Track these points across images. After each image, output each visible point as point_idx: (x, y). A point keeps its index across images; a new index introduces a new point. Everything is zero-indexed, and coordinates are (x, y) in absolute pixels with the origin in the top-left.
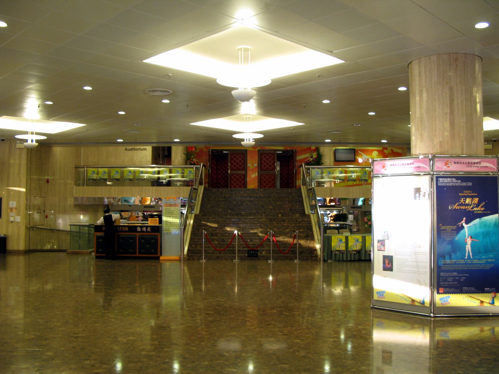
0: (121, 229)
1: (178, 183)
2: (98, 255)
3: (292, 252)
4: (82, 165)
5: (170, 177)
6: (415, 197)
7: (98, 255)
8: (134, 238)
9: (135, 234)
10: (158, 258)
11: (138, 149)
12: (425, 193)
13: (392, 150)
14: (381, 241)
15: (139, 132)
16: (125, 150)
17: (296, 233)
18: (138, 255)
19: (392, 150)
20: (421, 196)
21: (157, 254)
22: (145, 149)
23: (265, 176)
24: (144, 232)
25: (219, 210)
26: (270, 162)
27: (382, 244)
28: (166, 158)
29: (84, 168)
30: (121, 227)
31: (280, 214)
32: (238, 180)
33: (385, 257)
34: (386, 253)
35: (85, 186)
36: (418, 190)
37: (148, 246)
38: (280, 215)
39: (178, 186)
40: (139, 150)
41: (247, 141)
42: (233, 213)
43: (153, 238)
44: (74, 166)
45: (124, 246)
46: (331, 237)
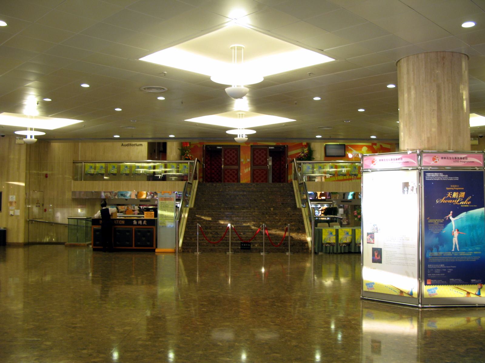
0: (117, 223)
1: (173, 178)
2: (95, 247)
3: (284, 245)
4: (79, 160)
5: (165, 172)
6: (404, 191)
7: (95, 247)
8: (130, 231)
9: (131, 227)
10: (154, 251)
11: (135, 144)
12: (413, 187)
13: (381, 146)
14: (371, 234)
16: (122, 145)
17: (288, 226)
18: (134, 247)
19: (381, 146)
20: (410, 190)
21: (152, 246)
22: (141, 144)
23: (258, 171)
24: (139, 225)
25: (213, 204)
26: (263, 157)
27: (371, 237)
28: (161, 153)
29: (82, 163)
30: (117, 221)
31: (272, 207)
32: (231, 174)
33: (374, 250)
34: (375, 246)
35: (83, 180)
36: (406, 185)
37: (144, 239)
38: (272, 209)
39: (173, 181)
40: (135, 145)
41: (240, 137)
42: (226, 206)
43: (149, 231)
44: (72, 161)
45: (121, 239)
46: (322, 230)
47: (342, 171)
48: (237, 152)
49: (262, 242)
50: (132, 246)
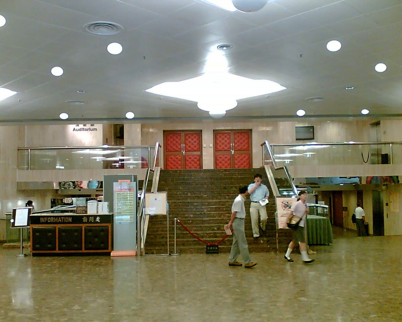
0: (63, 221)
1: (131, 166)
2: (34, 252)
3: (267, 242)
4: (26, 147)
5: (123, 160)
7: (34, 252)
8: (79, 231)
9: (81, 225)
10: (109, 254)
11: (88, 129)
15: (84, 104)
16: (74, 130)
18: (84, 251)
21: (108, 249)
22: (95, 129)
23: (221, 156)
24: (91, 223)
25: (178, 193)
26: (226, 141)
28: (118, 139)
29: (28, 149)
30: (62, 218)
32: (193, 161)
35: (29, 169)
37: (96, 240)
39: (117, 168)
40: (89, 130)
42: (193, 195)
43: (103, 231)
44: (17, 149)
45: (70, 239)
47: (116, 165)
48: (230, 137)
49: (173, 240)
50: (55, 250)
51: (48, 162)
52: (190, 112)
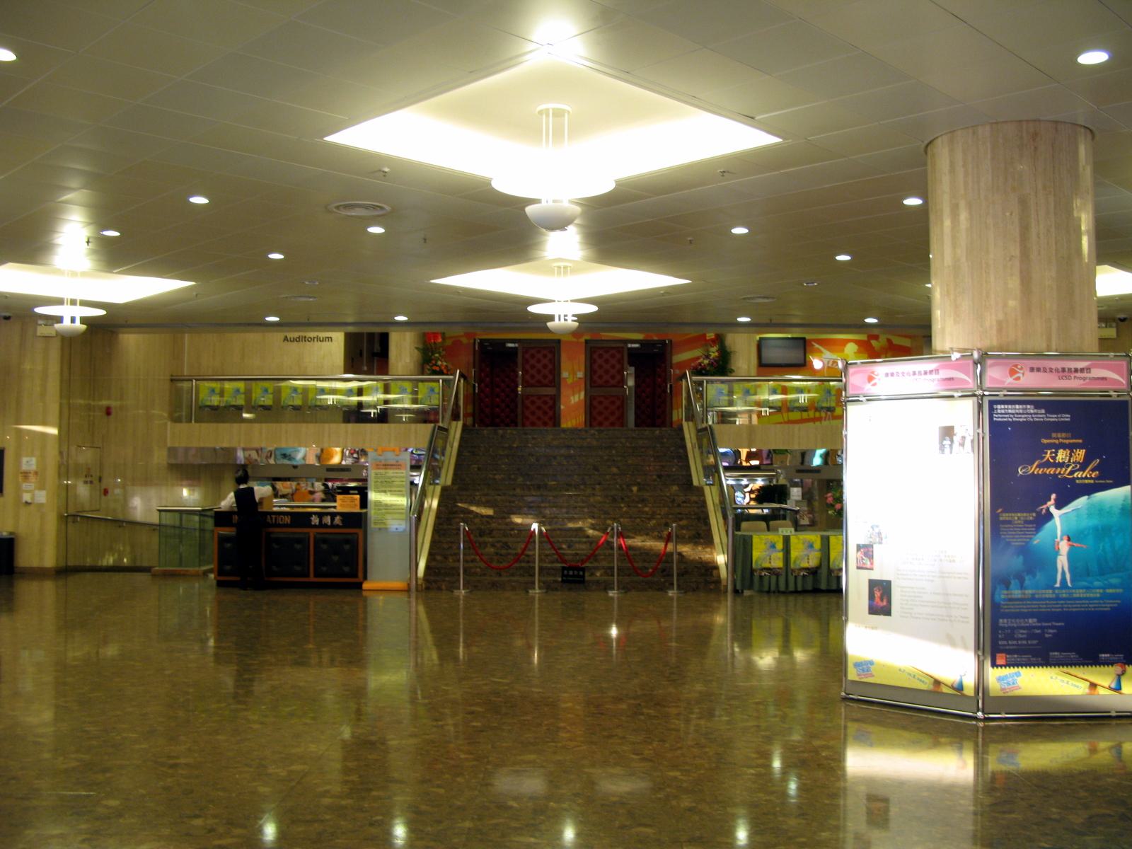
0: (274, 521)
1: (404, 416)
2: (222, 578)
3: (662, 572)
4: (185, 374)
5: (386, 402)
6: (942, 448)
7: (222, 578)
8: (303, 541)
9: (305, 530)
10: (359, 586)
11: (314, 338)
12: (964, 438)
13: (889, 341)
14: (865, 546)
15: (315, 299)
16: (284, 340)
17: (672, 529)
18: (312, 579)
19: (889, 341)
20: (956, 445)
21: (356, 576)
22: (328, 338)
23: (602, 399)
24: (326, 526)
25: (497, 477)
26: (613, 367)
27: (866, 554)
28: (375, 358)
29: (192, 380)
30: (274, 516)
31: (635, 485)
32: (539, 408)
33: (873, 584)
34: (876, 575)
35: (193, 422)
36: (948, 432)
37: (336, 558)
38: (635, 489)
40: (315, 340)
41: (560, 320)
42: (528, 483)
43: (347, 541)
44: (169, 378)
45: (282, 558)
46: (751, 537)
47: (797, 400)
51: (404, 420)
52: (514, 311)
